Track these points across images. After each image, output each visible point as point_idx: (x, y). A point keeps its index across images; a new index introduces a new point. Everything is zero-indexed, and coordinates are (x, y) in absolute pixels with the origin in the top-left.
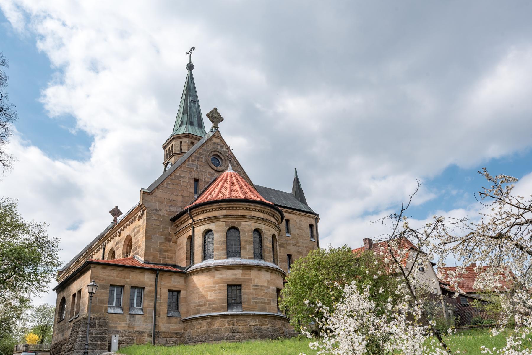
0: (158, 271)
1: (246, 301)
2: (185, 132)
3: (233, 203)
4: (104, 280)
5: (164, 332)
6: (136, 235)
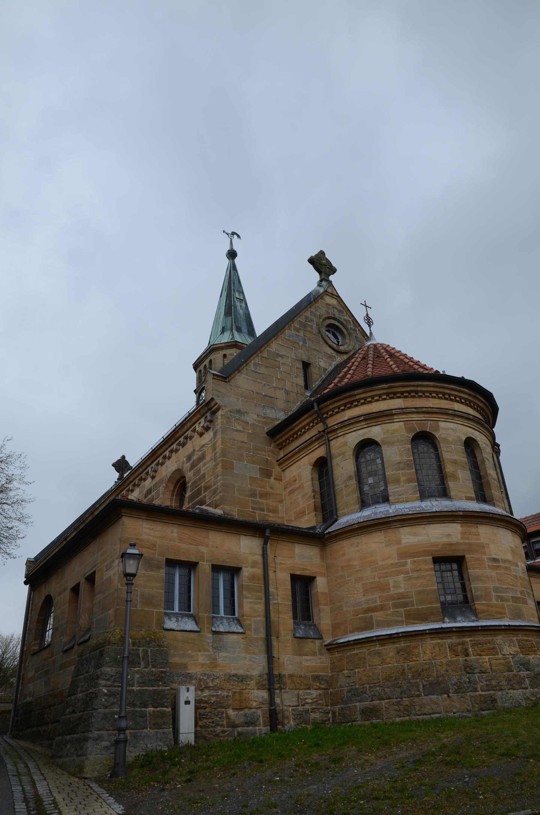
2: (231, 339)
3: (416, 383)
4: (153, 546)
5: (291, 676)
6: (196, 465)
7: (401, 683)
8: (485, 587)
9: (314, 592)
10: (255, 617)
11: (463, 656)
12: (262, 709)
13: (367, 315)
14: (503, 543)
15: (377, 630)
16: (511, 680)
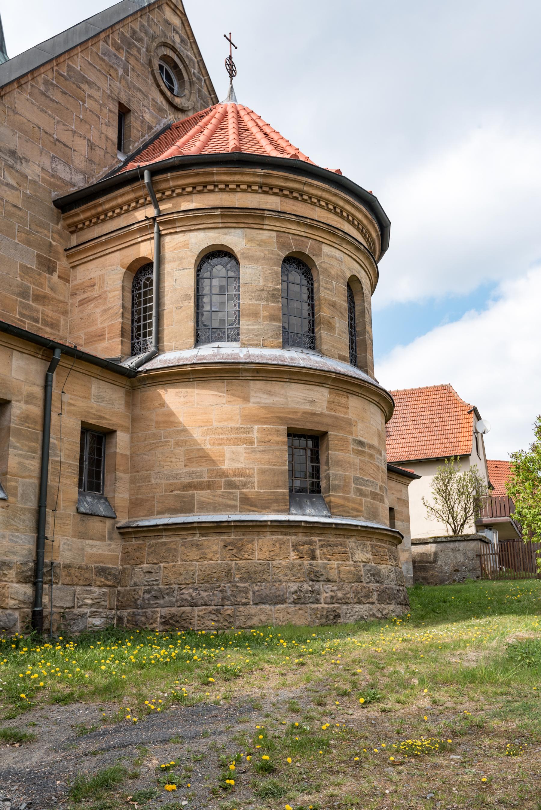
0: (58, 352)
1: (339, 486)
3: (305, 179)
5: (67, 567)
7: (224, 587)
8: (345, 475)
9: (109, 451)
10: (24, 477)
11: (309, 559)
12: (22, 610)
13: (230, 57)
14: (372, 423)
15: (198, 514)
16: (358, 593)
